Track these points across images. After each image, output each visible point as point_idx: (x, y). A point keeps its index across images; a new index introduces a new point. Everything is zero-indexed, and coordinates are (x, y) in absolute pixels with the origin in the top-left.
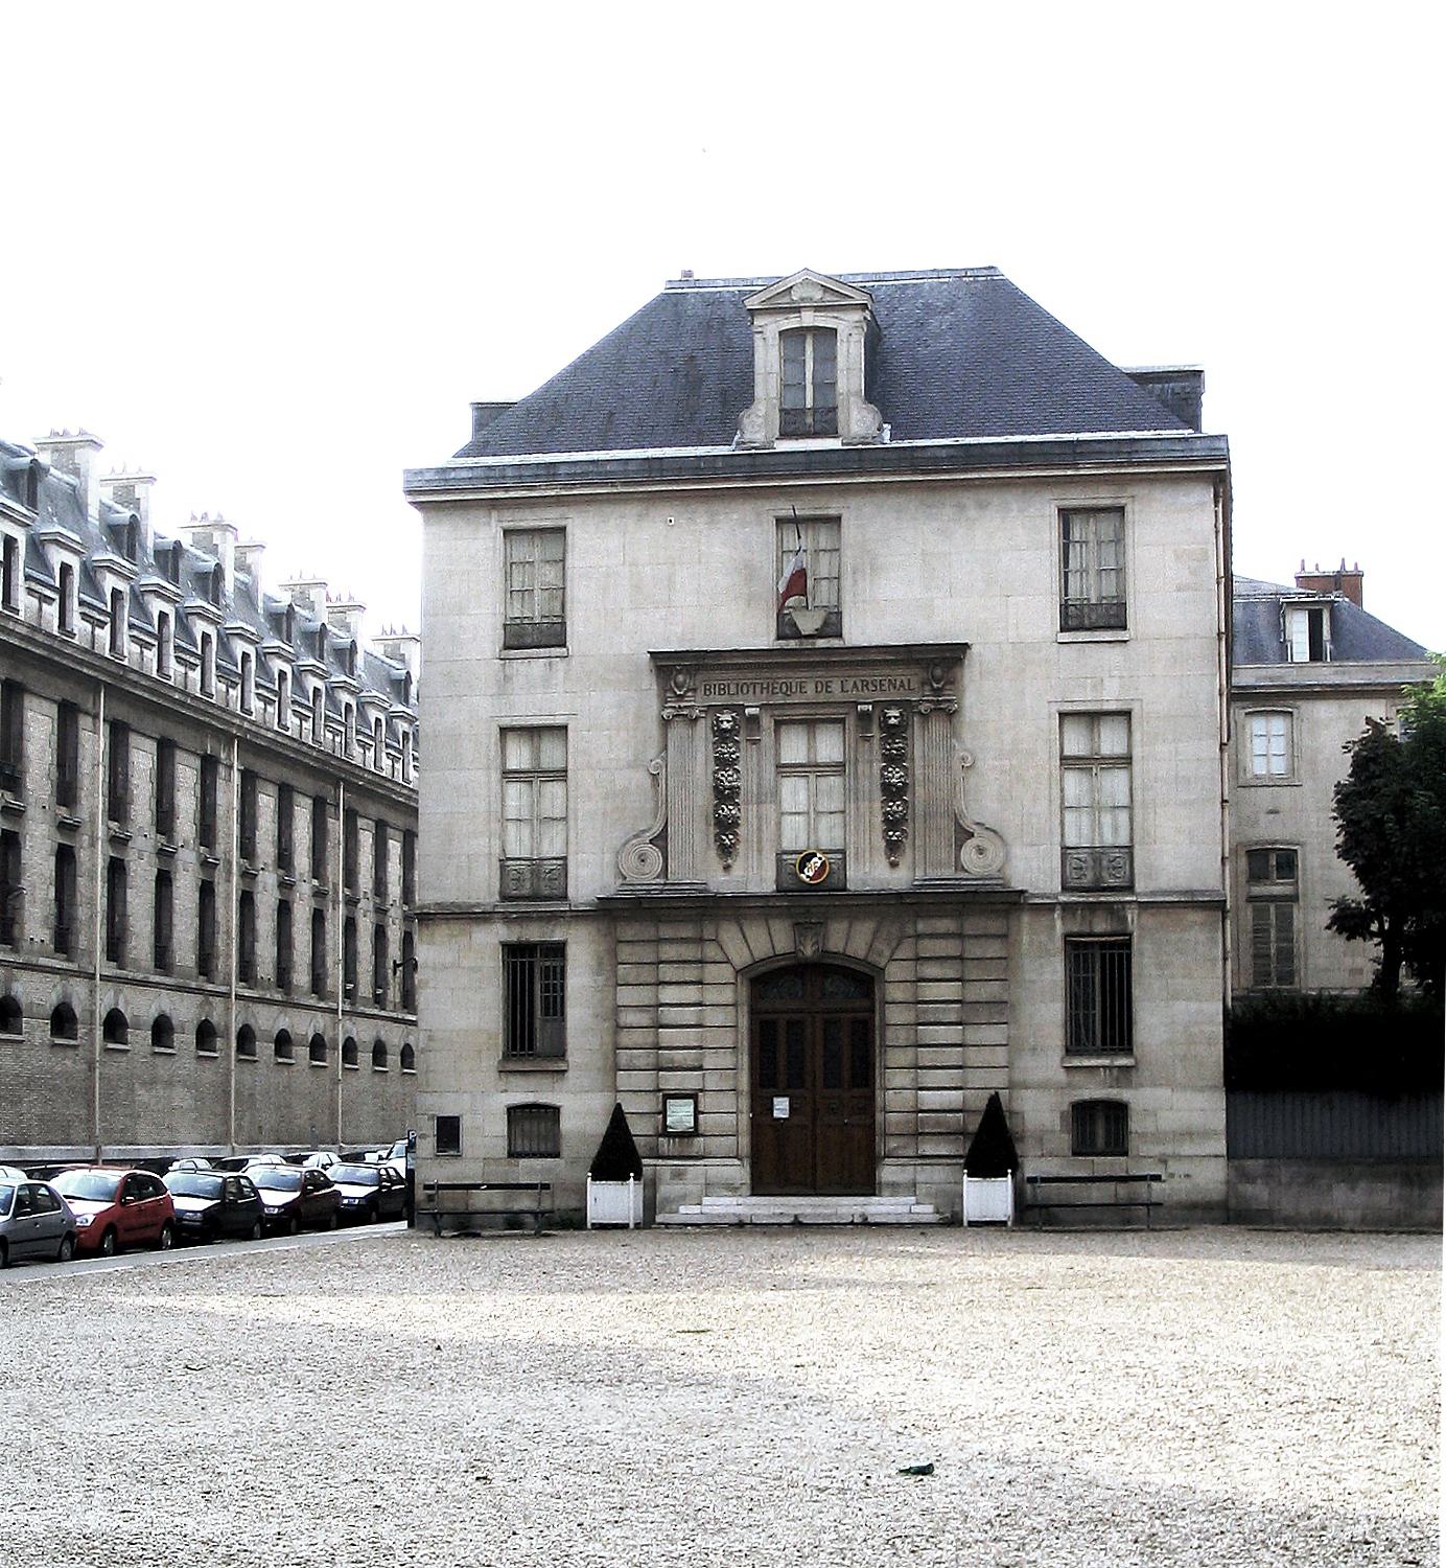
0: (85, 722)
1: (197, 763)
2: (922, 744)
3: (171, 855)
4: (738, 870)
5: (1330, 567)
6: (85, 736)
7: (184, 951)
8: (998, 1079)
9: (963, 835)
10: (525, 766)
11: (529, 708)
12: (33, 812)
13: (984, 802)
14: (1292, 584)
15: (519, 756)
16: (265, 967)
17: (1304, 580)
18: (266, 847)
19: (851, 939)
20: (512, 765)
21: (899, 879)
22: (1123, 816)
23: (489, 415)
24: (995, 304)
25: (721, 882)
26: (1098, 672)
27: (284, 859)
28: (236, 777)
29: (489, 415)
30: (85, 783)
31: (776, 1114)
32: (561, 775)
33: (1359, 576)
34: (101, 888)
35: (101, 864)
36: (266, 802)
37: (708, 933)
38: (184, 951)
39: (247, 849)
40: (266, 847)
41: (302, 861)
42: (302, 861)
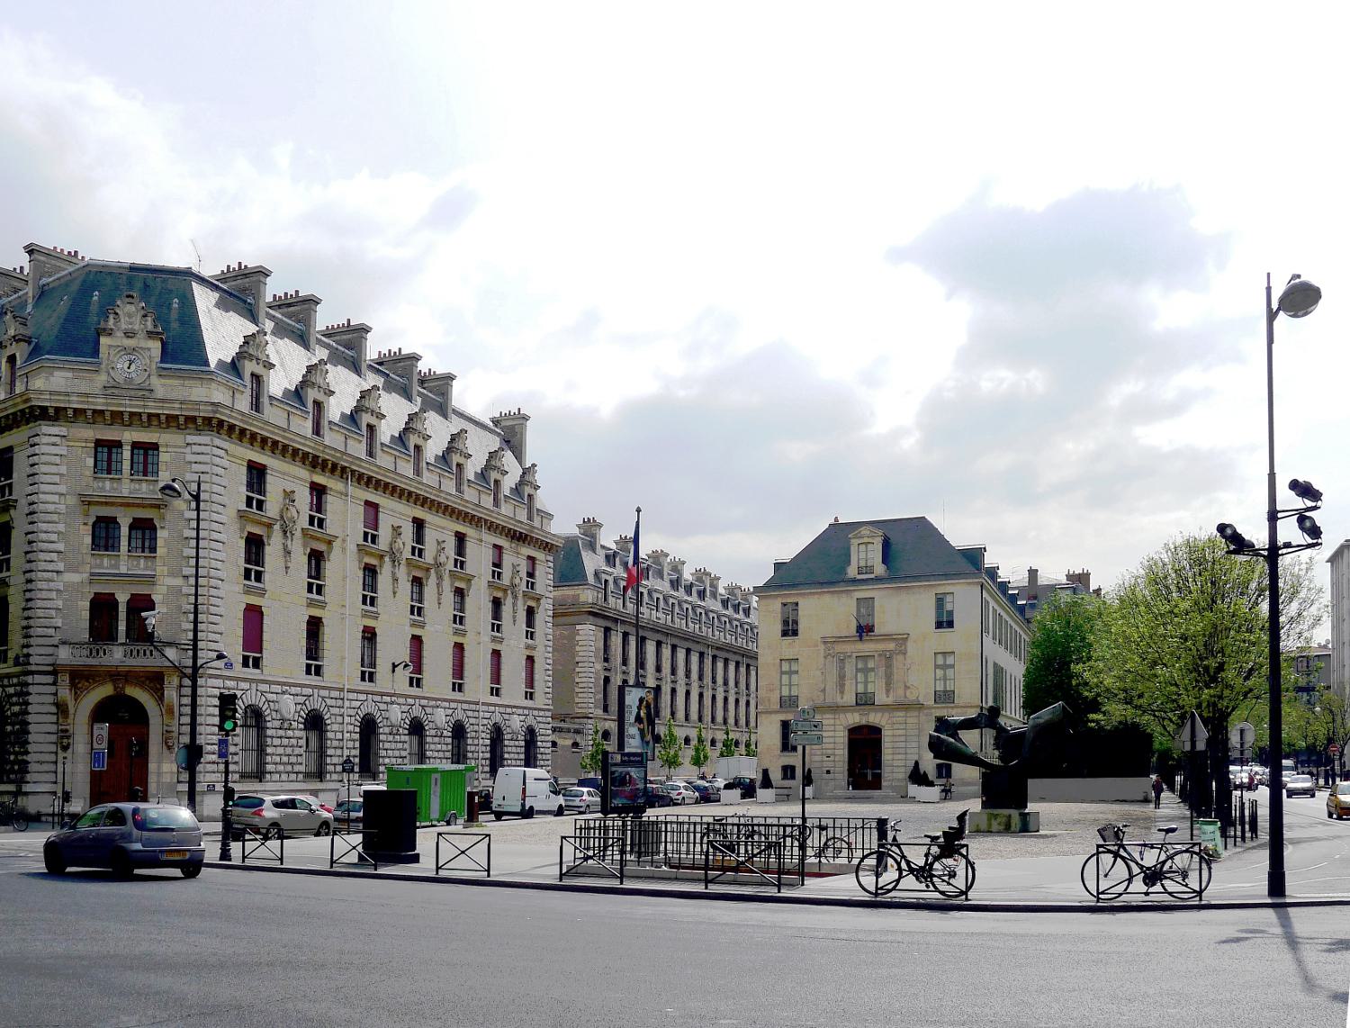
0: (664, 646)
1: (698, 655)
2: (898, 661)
3: (690, 685)
4: (845, 697)
5: (1078, 571)
6: (664, 650)
7: (694, 716)
8: (916, 758)
9: (907, 687)
10: (787, 670)
11: (788, 654)
12: (649, 676)
13: (913, 679)
14: (1065, 581)
15: (786, 667)
16: (719, 718)
17: (1069, 577)
18: (720, 680)
19: (874, 718)
20: (784, 669)
21: (889, 700)
22: (952, 681)
23: (778, 566)
24: (921, 527)
25: (839, 701)
26: (947, 639)
27: (726, 683)
28: (710, 658)
29: (778, 566)
30: (664, 665)
31: (1284, 761)
32: (797, 672)
33: (1088, 575)
34: (669, 697)
35: (669, 690)
36: (720, 665)
37: (837, 717)
38: (694, 716)
39: (714, 681)
40: (720, 680)
41: (732, 683)
42: (732, 683)
